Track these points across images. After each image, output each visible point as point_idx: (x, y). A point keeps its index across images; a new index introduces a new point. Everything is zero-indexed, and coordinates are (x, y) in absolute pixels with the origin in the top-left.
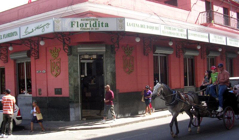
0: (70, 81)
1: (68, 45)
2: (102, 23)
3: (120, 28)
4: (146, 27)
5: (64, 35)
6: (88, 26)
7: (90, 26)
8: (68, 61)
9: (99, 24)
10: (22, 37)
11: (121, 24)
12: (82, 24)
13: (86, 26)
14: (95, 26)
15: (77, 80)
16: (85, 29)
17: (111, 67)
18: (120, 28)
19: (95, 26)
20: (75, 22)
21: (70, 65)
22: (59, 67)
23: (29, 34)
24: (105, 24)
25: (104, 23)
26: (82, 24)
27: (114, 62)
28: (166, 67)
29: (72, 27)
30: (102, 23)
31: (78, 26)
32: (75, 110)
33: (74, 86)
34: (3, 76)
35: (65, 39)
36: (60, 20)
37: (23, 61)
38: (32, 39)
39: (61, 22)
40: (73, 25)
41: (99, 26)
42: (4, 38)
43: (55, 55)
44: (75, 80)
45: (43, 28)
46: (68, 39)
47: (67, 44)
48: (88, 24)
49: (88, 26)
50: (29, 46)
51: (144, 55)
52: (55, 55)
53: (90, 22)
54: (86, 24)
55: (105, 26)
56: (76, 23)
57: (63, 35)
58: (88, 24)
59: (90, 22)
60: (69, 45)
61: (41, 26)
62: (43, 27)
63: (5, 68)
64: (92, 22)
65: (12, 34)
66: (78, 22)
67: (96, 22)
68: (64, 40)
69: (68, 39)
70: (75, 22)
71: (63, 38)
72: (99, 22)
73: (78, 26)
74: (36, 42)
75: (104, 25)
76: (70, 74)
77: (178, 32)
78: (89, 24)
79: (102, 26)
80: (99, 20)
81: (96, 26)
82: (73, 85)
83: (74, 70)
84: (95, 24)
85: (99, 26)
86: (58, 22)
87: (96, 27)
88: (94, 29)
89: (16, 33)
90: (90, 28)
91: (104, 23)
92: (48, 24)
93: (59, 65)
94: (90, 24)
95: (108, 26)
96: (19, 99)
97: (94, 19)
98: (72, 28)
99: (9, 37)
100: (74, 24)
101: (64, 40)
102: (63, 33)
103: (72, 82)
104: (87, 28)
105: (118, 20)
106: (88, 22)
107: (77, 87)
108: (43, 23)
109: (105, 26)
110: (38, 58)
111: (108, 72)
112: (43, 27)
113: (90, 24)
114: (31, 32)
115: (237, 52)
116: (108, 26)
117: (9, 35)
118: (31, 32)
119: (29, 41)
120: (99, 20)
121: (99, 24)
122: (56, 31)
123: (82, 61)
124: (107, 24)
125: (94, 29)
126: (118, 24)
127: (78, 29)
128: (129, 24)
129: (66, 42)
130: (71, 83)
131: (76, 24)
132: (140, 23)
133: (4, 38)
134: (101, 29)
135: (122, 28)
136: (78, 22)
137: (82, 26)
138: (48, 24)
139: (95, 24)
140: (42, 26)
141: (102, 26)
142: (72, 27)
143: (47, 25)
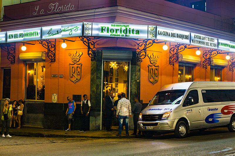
0: (91, 88)
1: (92, 50)
8: (91, 67)
15: (100, 88)
21: (92, 71)
22: (80, 73)
28: (70, 138)
32: (95, 118)
33: (96, 93)
43: (154, 61)
47: (91, 49)
52: (154, 61)
57: (88, 39)
62: (70, 30)
63: (11, 69)
74: (53, 43)
77: (207, 41)
82: (95, 92)
83: (97, 77)
112: (70, 30)
115: (162, 48)
119: (47, 42)
128: (160, 32)
129: (92, 47)
130: (93, 89)
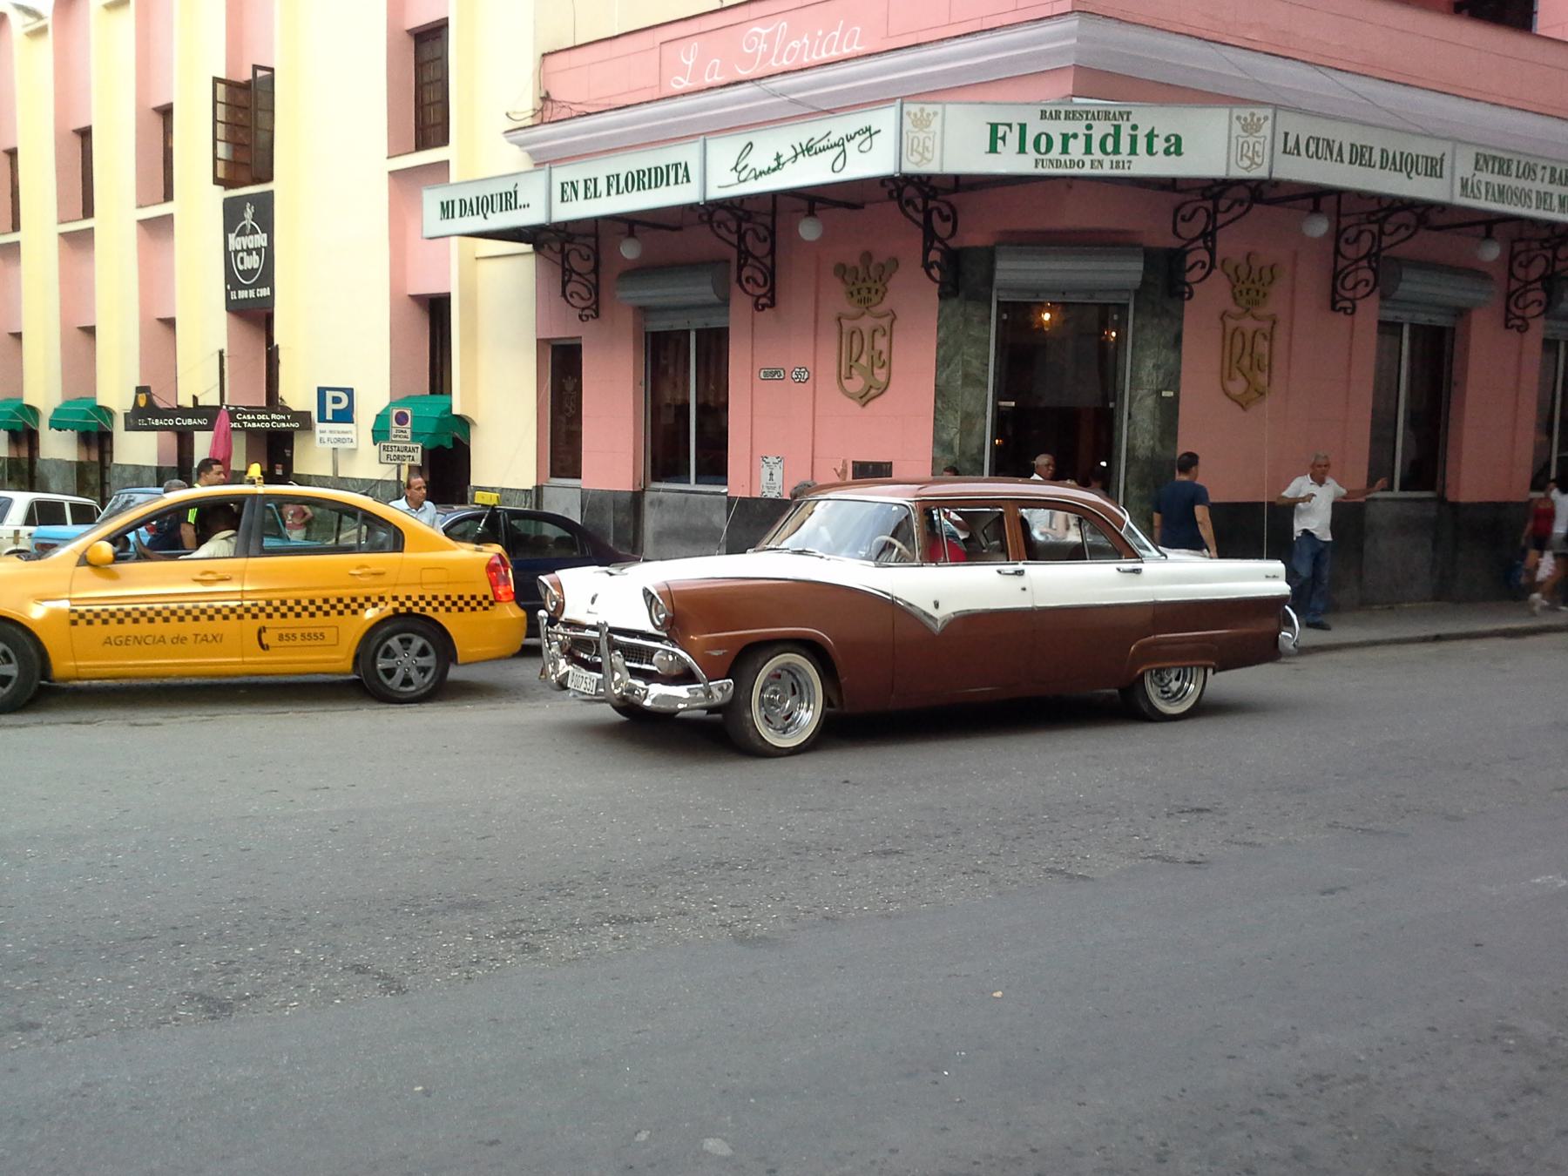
2: (1151, 136)
3: (1247, 163)
4: (1376, 156)
5: (932, 188)
6: (1076, 147)
7: (1088, 151)
9: (1134, 139)
10: (715, 193)
11: (1251, 140)
12: (1044, 138)
13: (1065, 150)
14: (1110, 148)
15: (978, 428)
16: (1058, 164)
17: (1157, 367)
18: (1247, 163)
19: (1110, 148)
20: (1010, 125)
23: (756, 177)
24: (1167, 140)
25: (1162, 132)
26: (1044, 138)
27: (1178, 340)
29: (993, 149)
30: (1151, 136)
31: (1022, 150)
33: (963, 453)
34: (569, 387)
35: (935, 215)
36: (935, 114)
37: (679, 325)
38: (747, 207)
39: (936, 124)
40: (1000, 142)
41: (1133, 152)
42: (613, 191)
44: (968, 419)
45: (838, 150)
46: (946, 211)
48: (1075, 136)
49: (1076, 147)
50: (734, 239)
51: (1333, 308)
53: (1089, 127)
54: (1066, 138)
55: (1167, 152)
56: (1016, 129)
58: (1075, 136)
59: (1089, 127)
60: (952, 243)
61: (824, 143)
62: (837, 145)
64: (1101, 128)
65: (659, 176)
66: (1023, 127)
67: (1117, 128)
68: (741, 238)
69: (946, 211)
70: (1010, 125)
71: (739, 226)
72: (1134, 127)
73: (1022, 150)
75: (1159, 145)
76: (940, 393)
78: (1082, 139)
79: (1150, 151)
80: (1133, 121)
81: (1116, 151)
83: (966, 376)
84: (1110, 141)
85: (1133, 152)
86: (922, 123)
87: (1115, 158)
88: (1107, 164)
89: (681, 172)
90: (1087, 159)
91: (1162, 132)
92: (869, 129)
93: (881, 343)
94: (1089, 138)
95: (1178, 153)
96: (652, 503)
97: (1107, 114)
98: (993, 156)
99: (641, 186)
100: (1003, 139)
101: (741, 238)
102: (737, 203)
103: (952, 433)
104: (1067, 157)
105: (1238, 118)
106: (1078, 127)
107: (975, 460)
108: (840, 126)
109: (1167, 152)
110: (772, 304)
111: (1141, 393)
112: (837, 145)
113: (1089, 138)
114: (770, 171)
116: (1178, 153)
117: (638, 181)
118: (770, 171)
120: (1133, 121)
121: (1134, 139)
122: (910, 168)
123: (329, 416)
124: (1178, 139)
125: (1107, 164)
126: (1234, 141)
127: (1024, 165)
128: (1291, 143)
129: (942, 228)
130: (945, 437)
131: (1013, 138)
132: (1345, 136)
133: (613, 191)
134: (1144, 166)
135: (1253, 162)
136: (1023, 127)
137: (1043, 149)
138: (869, 129)
139: (1110, 141)
140: (834, 139)
141: (1150, 151)
142: (993, 149)
143: (859, 139)
